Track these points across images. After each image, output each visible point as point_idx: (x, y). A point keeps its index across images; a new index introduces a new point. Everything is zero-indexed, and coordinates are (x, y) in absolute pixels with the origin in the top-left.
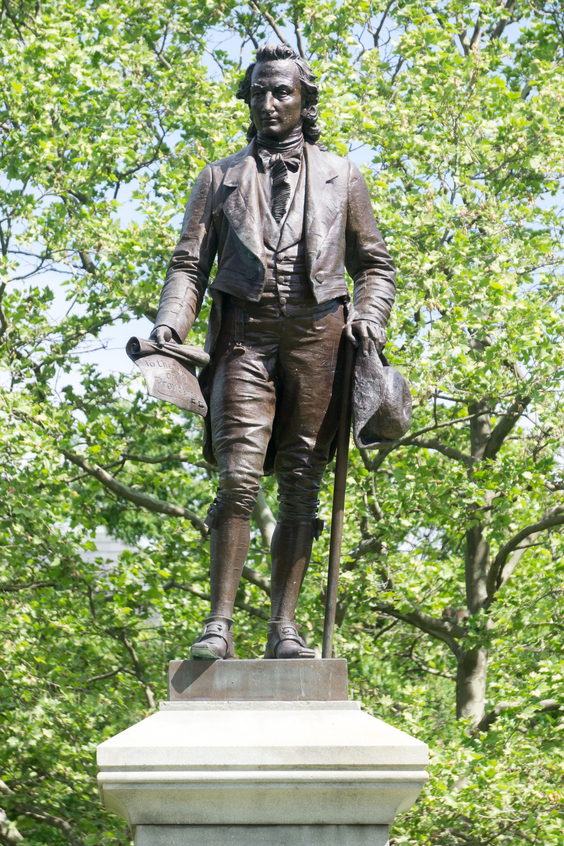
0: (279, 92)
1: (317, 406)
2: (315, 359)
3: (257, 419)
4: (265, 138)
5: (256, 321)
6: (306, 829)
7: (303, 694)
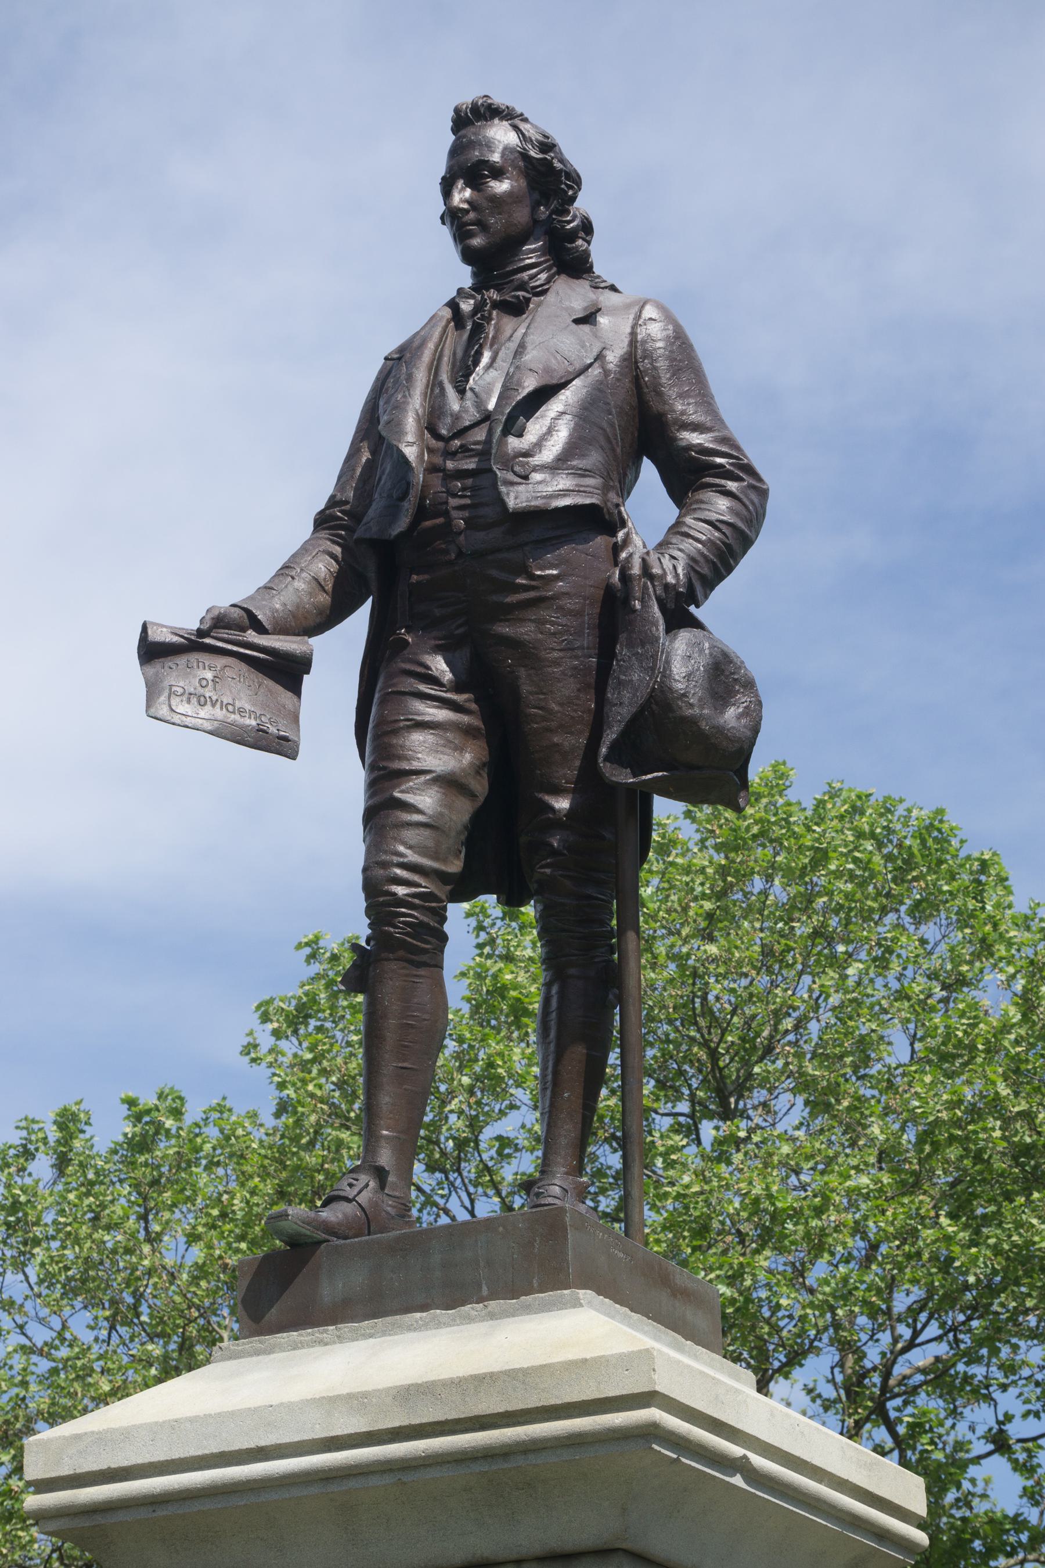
2: (551, 636)
5: (421, 577)
7: (485, 1291)
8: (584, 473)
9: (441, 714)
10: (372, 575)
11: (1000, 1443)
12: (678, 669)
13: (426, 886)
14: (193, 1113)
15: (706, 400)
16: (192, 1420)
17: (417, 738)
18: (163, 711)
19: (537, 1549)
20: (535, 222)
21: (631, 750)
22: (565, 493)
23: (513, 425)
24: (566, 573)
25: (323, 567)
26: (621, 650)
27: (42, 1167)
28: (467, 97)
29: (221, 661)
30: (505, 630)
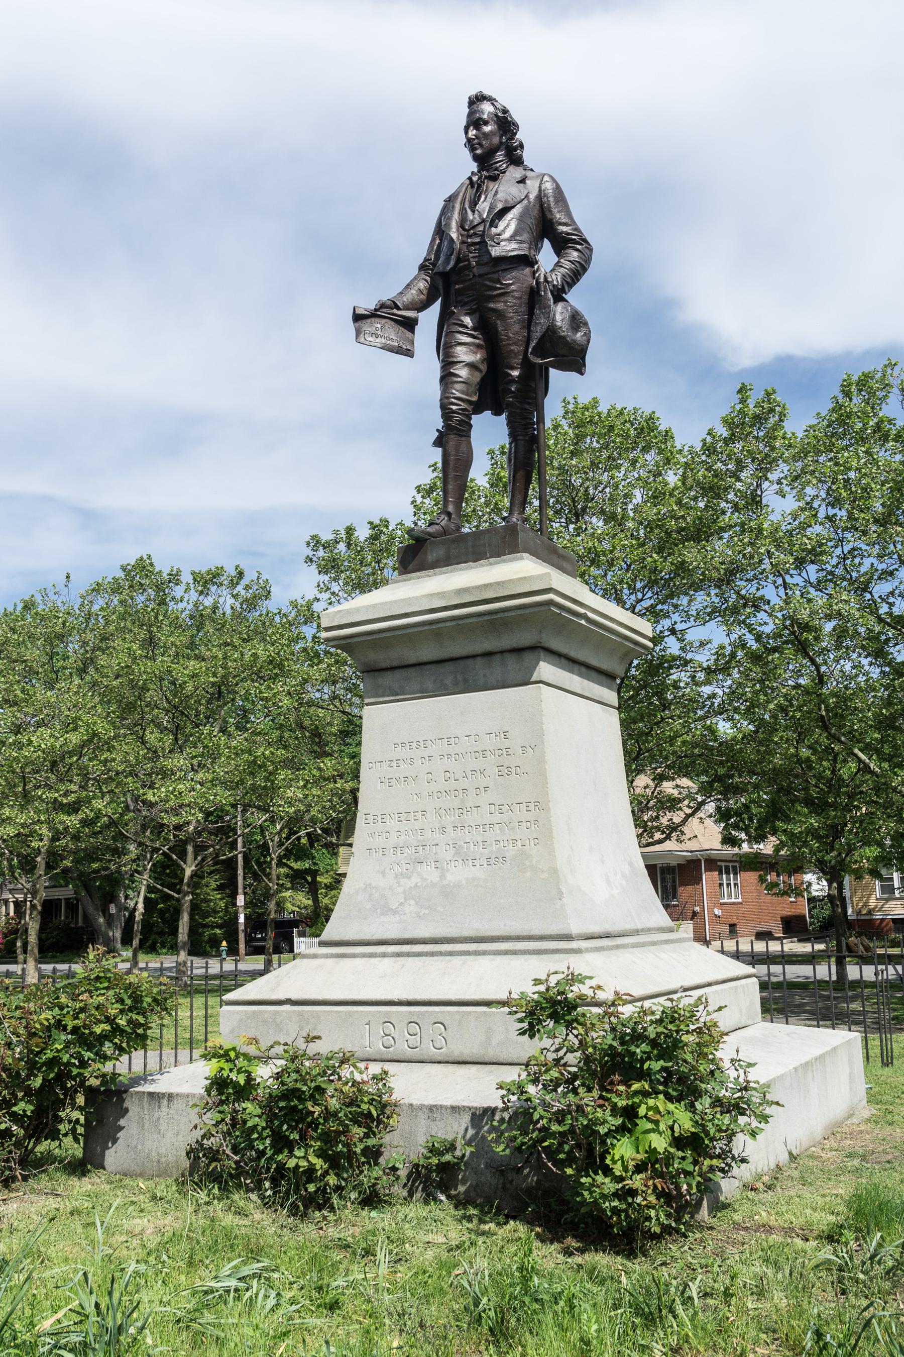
1: (515, 343)
2: (510, 307)
6: (479, 659)
8: (521, 242)
9: (468, 340)
10: (441, 287)
11: (673, 631)
12: (558, 318)
13: (464, 406)
14: (392, 526)
15: (569, 214)
16: (382, 604)
17: (459, 349)
18: (362, 340)
19: (509, 647)
20: (501, 143)
21: (540, 350)
22: (514, 250)
23: (493, 224)
24: (515, 282)
25: (422, 285)
26: (537, 311)
27: (342, 547)
28: (473, 92)
29: (384, 321)
30: (492, 305)
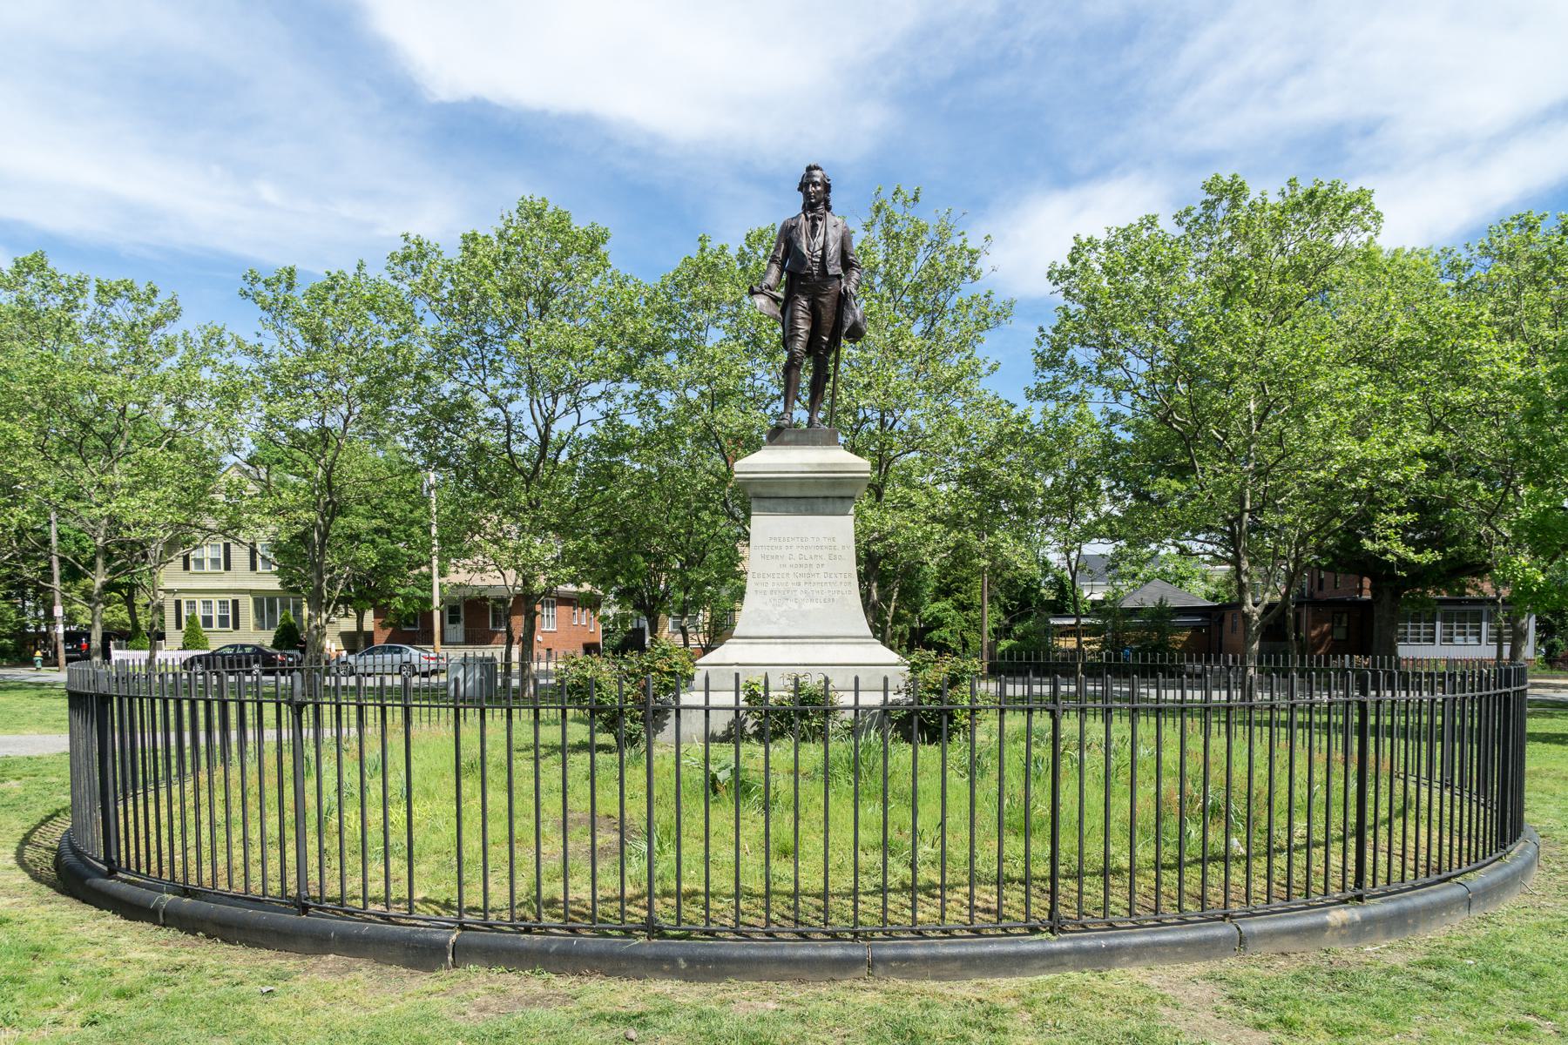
0: (815, 184)
3: (803, 327)
4: (809, 206)
